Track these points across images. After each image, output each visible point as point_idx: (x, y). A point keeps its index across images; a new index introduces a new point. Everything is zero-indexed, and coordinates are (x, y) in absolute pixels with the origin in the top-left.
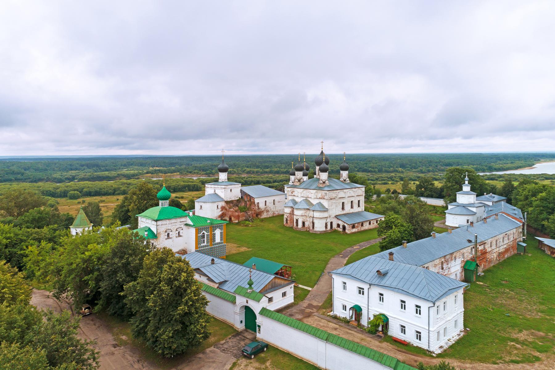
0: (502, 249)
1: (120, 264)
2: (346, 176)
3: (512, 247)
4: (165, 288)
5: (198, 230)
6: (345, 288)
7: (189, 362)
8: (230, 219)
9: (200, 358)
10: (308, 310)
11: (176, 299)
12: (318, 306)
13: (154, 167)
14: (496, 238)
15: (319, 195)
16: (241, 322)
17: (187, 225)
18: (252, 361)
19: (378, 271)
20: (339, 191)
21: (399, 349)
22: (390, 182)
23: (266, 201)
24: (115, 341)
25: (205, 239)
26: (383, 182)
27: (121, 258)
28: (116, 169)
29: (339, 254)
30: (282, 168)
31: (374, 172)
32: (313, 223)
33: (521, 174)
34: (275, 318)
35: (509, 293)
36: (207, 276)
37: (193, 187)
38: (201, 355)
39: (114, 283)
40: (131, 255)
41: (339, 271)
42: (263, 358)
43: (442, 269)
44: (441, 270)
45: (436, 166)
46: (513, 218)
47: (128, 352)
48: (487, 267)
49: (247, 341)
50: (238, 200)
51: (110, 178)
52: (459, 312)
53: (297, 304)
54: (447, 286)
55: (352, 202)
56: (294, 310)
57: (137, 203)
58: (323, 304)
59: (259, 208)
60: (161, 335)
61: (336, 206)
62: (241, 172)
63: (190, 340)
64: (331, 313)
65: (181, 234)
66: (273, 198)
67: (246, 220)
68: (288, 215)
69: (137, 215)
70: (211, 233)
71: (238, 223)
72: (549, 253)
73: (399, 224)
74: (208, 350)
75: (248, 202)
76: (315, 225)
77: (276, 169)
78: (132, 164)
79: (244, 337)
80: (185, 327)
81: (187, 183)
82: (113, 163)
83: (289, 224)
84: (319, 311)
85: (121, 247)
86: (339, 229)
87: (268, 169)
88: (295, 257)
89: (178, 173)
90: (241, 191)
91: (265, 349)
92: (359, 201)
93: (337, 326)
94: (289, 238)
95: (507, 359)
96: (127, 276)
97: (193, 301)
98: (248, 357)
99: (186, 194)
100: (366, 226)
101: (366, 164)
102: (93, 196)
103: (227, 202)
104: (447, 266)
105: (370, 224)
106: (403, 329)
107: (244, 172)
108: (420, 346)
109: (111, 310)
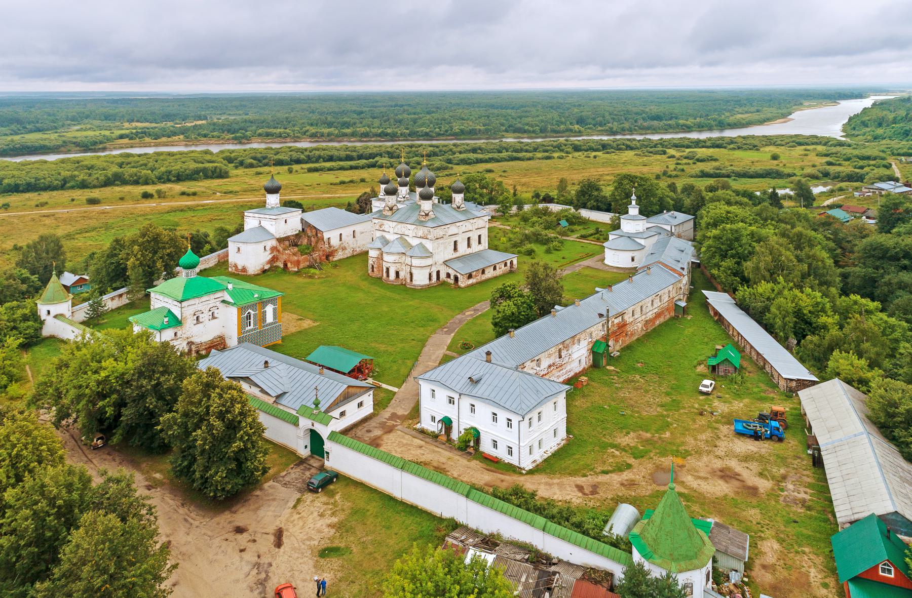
0: (650, 316)
1: (149, 387)
2: (460, 201)
3: (667, 310)
4: (217, 423)
5: (241, 310)
6: (433, 396)
7: (245, 501)
8: (285, 265)
9: (257, 496)
10: (390, 423)
11: (228, 433)
12: (404, 415)
13: (132, 121)
14: (640, 304)
15: (420, 234)
16: (306, 447)
17: (224, 301)
18: (318, 495)
19: (470, 378)
20: (448, 226)
21: (488, 468)
22: (556, 155)
23: (341, 234)
24: (147, 481)
25: (252, 321)
26: (546, 154)
27: (150, 378)
28: (56, 128)
29: (442, 327)
30: (373, 128)
31: (534, 132)
32: (411, 274)
33: (763, 136)
34: (345, 444)
35: (638, 382)
36: (260, 387)
37: (212, 172)
38: (258, 493)
39: (141, 410)
40: (163, 373)
41: (427, 376)
42: (332, 491)
43: (560, 357)
44: (558, 359)
45: (636, 121)
46: (671, 270)
47: (168, 495)
48: (627, 343)
49: (313, 471)
50: (297, 235)
51: (49, 149)
52: (559, 419)
53: (378, 415)
54: (544, 393)
55: (469, 238)
56: (373, 423)
57: (139, 256)
58: (410, 413)
59: (330, 247)
60: (212, 476)
61: (445, 248)
62: (299, 135)
63: (247, 479)
64: (418, 426)
65: (216, 315)
66: (351, 229)
67: (310, 267)
68: (374, 260)
69: (148, 290)
70: (260, 312)
71: (297, 272)
72: (713, 314)
73: (516, 295)
74: (266, 486)
75: (312, 239)
76: (414, 278)
77: (363, 130)
78: (87, 117)
79: (310, 465)
80: (240, 464)
81: (201, 165)
82: (49, 115)
83: (376, 273)
84: (404, 423)
85: (149, 364)
86: (449, 280)
87: (348, 128)
88: (381, 335)
89: (182, 137)
90: (302, 220)
91: (335, 480)
92: (480, 236)
93: (423, 443)
94: (375, 300)
95: (599, 469)
96: (158, 399)
97: (248, 435)
98: (314, 491)
99: (200, 184)
100: (490, 273)
101: (520, 117)
102: (23, 192)
103: (280, 240)
104: (566, 353)
105: (495, 269)
106: (495, 444)
107: (305, 134)
108: (511, 462)
109: (135, 440)
